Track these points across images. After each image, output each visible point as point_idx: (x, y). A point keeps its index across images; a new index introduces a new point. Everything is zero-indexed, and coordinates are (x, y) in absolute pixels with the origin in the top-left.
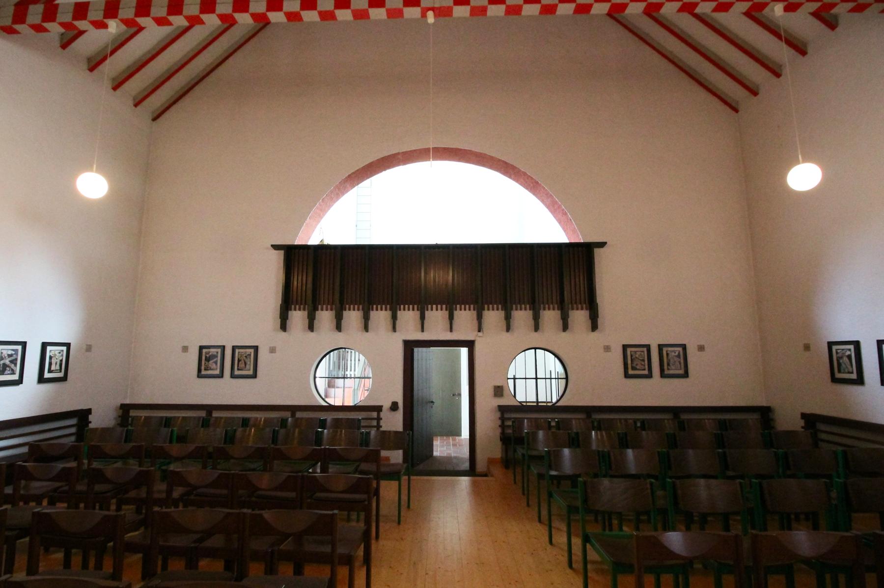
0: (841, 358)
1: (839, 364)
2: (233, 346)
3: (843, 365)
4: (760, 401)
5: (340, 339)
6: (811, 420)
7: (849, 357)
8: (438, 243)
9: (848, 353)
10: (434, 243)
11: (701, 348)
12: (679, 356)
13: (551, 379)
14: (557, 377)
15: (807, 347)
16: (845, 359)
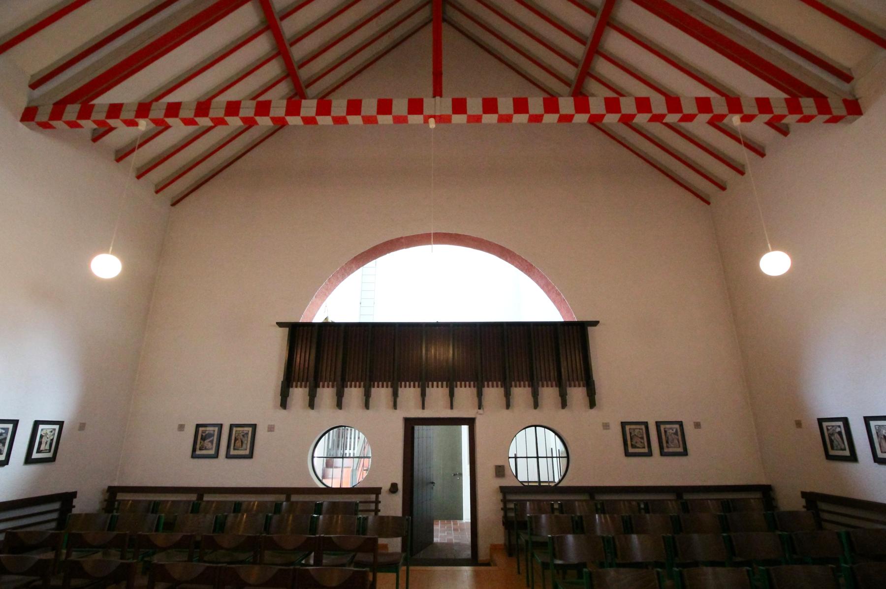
0: (833, 434)
1: (832, 441)
2: (622, 423)
3: (835, 443)
4: (764, 481)
5: (340, 417)
6: (812, 499)
7: (840, 433)
8: (439, 321)
9: (838, 430)
10: (435, 321)
11: (697, 425)
12: (676, 433)
13: (552, 457)
14: (558, 456)
15: (799, 424)
16: (837, 436)
